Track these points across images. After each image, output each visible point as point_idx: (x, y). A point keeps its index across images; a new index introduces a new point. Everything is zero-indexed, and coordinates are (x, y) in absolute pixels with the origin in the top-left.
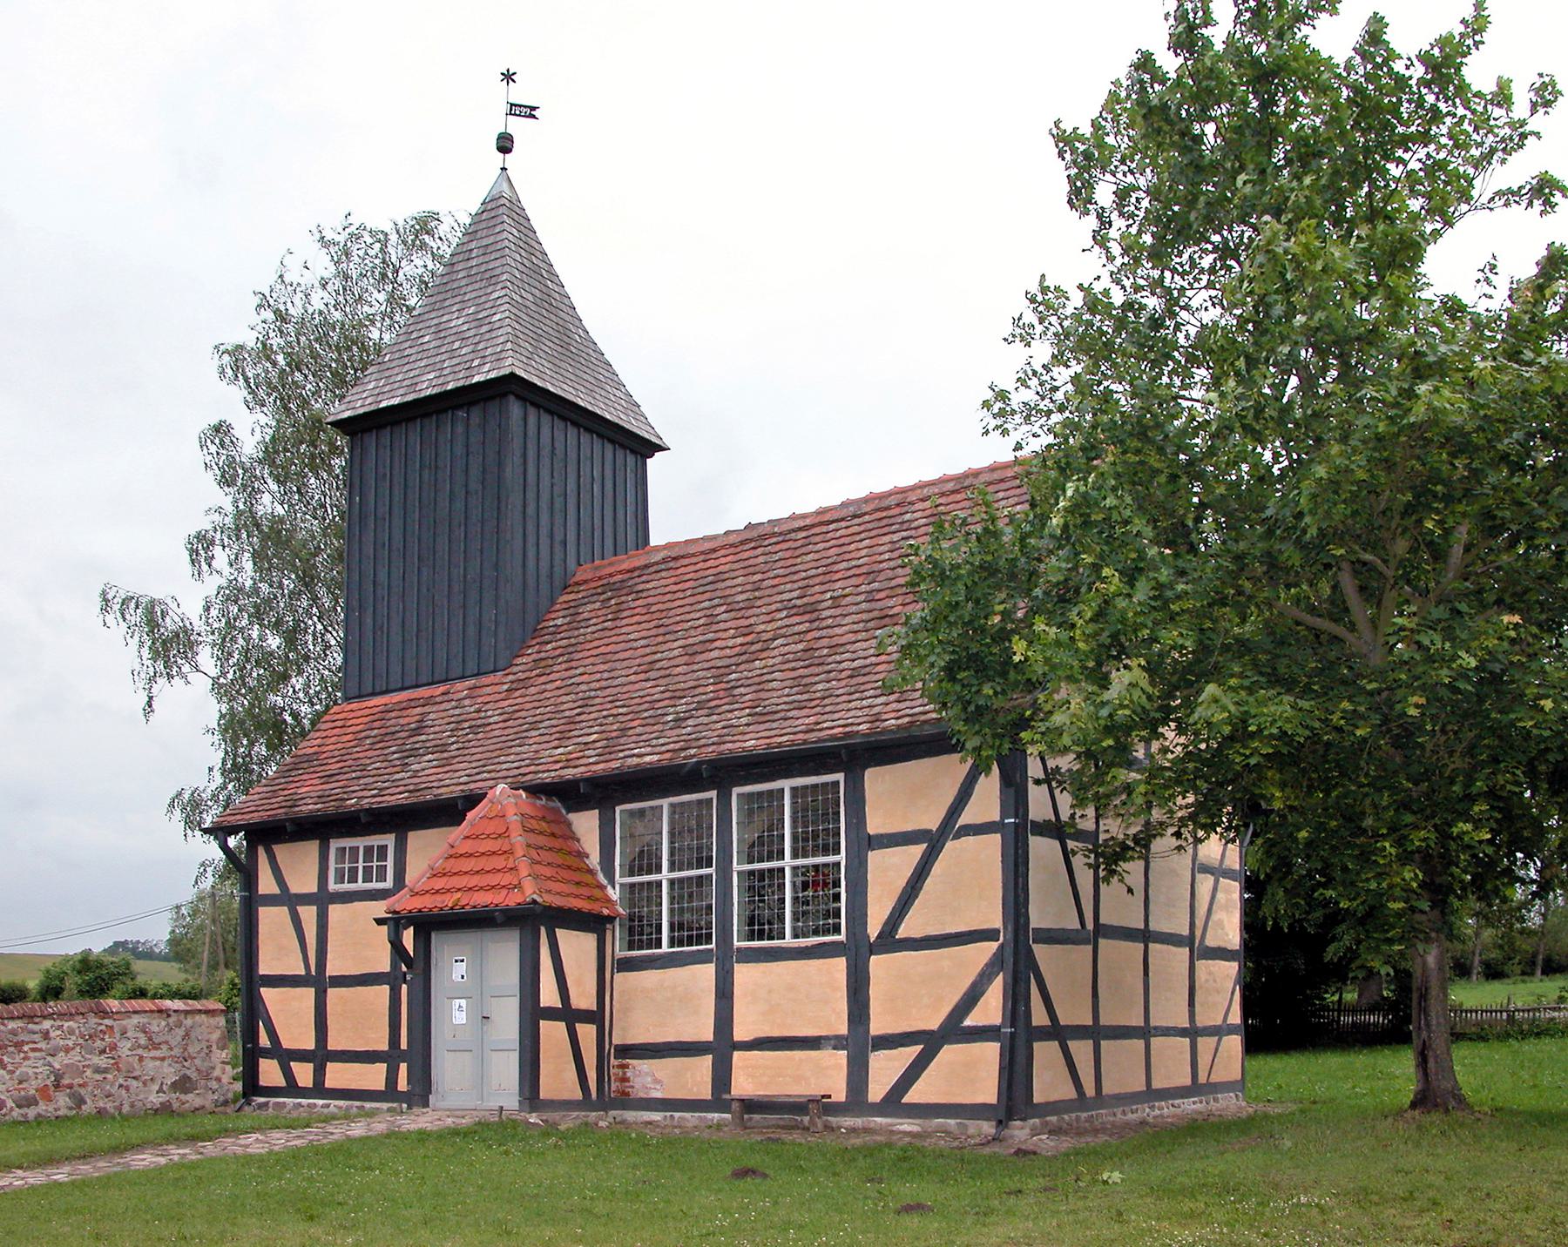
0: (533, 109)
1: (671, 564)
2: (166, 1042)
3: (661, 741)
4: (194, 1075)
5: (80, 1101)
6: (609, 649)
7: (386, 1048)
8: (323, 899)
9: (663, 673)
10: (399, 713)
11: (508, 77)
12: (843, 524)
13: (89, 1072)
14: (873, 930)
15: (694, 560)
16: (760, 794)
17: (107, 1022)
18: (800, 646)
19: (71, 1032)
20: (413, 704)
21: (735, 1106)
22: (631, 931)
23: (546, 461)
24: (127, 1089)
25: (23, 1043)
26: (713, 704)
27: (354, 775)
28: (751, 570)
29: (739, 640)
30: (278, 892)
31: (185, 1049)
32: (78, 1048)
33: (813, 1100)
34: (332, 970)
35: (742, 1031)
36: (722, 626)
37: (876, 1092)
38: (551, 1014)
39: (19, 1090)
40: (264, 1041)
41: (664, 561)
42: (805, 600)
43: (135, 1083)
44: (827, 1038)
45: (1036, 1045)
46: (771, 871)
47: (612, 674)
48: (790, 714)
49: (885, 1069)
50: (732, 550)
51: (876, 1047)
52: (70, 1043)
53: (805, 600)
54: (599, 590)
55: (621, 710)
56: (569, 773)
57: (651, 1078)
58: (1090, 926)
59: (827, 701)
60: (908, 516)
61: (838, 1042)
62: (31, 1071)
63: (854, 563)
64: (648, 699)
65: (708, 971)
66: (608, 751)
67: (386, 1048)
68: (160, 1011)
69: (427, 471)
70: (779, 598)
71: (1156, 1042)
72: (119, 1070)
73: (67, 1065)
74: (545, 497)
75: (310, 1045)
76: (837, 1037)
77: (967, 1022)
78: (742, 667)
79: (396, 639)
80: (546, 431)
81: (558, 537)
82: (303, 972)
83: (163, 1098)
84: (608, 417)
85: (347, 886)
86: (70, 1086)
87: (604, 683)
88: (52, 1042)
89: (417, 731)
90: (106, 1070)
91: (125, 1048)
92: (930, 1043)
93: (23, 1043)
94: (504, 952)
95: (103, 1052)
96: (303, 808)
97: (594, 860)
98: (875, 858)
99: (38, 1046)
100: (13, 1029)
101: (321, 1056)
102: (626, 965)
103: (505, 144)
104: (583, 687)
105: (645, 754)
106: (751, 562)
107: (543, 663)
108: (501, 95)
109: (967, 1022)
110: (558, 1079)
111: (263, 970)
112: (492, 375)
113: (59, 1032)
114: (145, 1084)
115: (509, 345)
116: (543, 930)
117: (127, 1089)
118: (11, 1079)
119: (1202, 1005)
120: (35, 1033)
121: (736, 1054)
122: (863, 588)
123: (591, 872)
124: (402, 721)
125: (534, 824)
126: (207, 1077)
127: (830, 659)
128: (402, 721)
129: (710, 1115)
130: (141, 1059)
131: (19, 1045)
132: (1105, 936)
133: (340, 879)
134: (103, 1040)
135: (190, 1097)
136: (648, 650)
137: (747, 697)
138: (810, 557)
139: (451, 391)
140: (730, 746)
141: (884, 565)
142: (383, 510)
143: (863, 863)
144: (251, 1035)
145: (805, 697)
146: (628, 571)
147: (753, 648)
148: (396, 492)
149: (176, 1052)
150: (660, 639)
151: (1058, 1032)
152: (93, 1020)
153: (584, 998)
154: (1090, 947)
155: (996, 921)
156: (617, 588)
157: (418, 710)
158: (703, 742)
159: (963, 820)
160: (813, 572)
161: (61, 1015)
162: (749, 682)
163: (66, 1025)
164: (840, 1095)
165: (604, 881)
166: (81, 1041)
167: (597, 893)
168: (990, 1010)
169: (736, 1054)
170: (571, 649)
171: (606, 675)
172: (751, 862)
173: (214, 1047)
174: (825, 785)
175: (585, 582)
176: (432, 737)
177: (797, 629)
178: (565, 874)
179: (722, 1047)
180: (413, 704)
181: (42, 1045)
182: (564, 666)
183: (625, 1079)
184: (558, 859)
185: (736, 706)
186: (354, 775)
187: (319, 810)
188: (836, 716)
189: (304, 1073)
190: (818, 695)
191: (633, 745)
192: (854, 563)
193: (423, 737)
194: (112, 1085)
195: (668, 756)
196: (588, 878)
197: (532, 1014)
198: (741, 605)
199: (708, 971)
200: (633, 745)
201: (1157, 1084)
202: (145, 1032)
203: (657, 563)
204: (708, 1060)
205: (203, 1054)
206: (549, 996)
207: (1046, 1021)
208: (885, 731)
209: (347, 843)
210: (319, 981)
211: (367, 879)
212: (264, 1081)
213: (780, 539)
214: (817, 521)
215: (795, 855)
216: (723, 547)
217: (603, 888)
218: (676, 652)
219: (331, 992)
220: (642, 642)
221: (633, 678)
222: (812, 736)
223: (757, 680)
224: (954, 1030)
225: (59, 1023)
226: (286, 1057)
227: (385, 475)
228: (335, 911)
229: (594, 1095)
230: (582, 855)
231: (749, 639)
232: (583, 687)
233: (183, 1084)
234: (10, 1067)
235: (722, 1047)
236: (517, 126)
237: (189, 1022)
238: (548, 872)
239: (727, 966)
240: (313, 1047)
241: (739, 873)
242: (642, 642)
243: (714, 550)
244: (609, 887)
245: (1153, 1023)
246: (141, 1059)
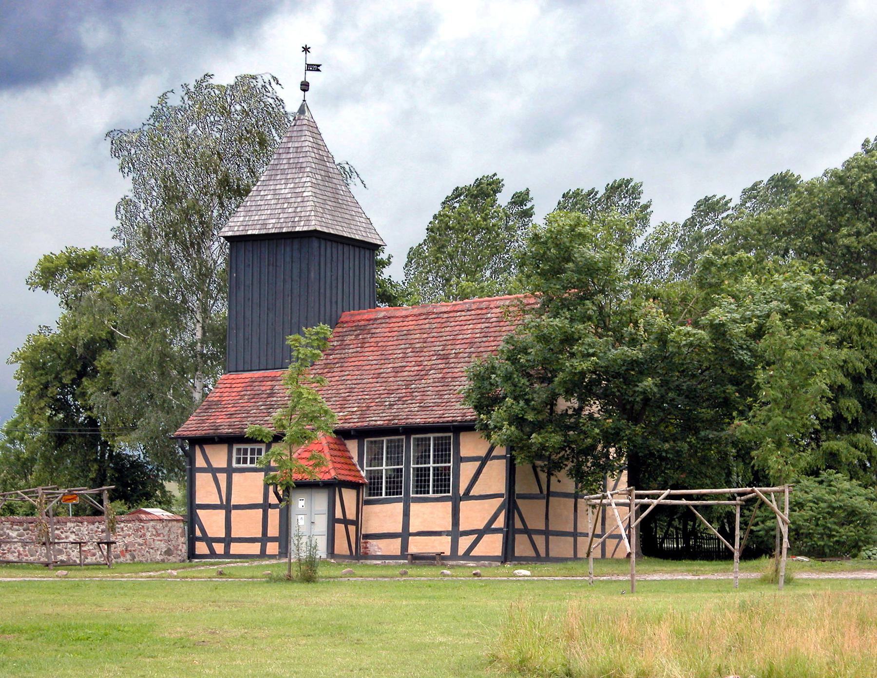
0: (319, 66)
1: (387, 320)
3: (384, 415)
5: (134, 557)
6: (360, 363)
7: (260, 536)
8: (229, 471)
9: (384, 380)
10: (260, 384)
11: (306, 49)
12: (463, 313)
14: (462, 492)
15: (398, 320)
16: (422, 439)
17: (142, 524)
18: (440, 376)
20: (266, 379)
21: (409, 557)
22: (370, 489)
23: (329, 265)
26: (404, 399)
27: (244, 415)
28: (423, 331)
29: (416, 368)
30: (217, 474)
33: (439, 554)
34: (234, 502)
35: (412, 529)
36: (410, 359)
37: (461, 551)
38: (339, 521)
40: (198, 533)
41: (384, 318)
42: (444, 352)
44: (444, 532)
45: (516, 535)
46: (425, 468)
47: (362, 377)
48: (434, 408)
49: (464, 543)
50: (415, 318)
51: (461, 535)
53: (444, 352)
54: (354, 329)
55: (367, 397)
56: (347, 425)
57: (377, 547)
58: (545, 492)
59: (448, 404)
60: (489, 315)
61: (448, 533)
63: (465, 336)
64: (378, 392)
66: (362, 417)
67: (260, 536)
69: (271, 267)
70: (434, 349)
74: (328, 281)
75: (222, 535)
76: (448, 532)
77: (493, 527)
78: (417, 382)
79: (255, 345)
80: (329, 251)
81: (334, 300)
82: (219, 503)
83: (162, 557)
84: (357, 237)
85: (242, 465)
86: (130, 551)
87: (358, 381)
89: (271, 395)
90: (142, 545)
92: (480, 534)
94: (321, 501)
95: (141, 537)
96: (223, 431)
97: (355, 460)
98: (462, 465)
101: (228, 540)
102: (368, 502)
104: (349, 382)
105: (377, 420)
106: (423, 326)
107: (329, 366)
108: (300, 60)
109: (493, 527)
110: (341, 547)
111: (198, 502)
112: (305, 229)
115: (313, 213)
116: (337, 489)
119: (609, 525)
121: (410, 538)
122: (467, 350)
123: (354, 465)
124: (262, 388)
125: (332, 446)
127: (451, 384)
128: (262, 388)
129: (400, 561)
130: (154, 540)
132: (552, 496)
133: (238, 462)
135: (171, 557)
136: (377, 367)
137: (418, 398)
138: (448, 329)
139: (285, 233)
140: (410, 420)
141: (476, 340)
142: (249, 282)
143: (459, 467)
144: (192, 531)
145: (440, 401)
146: (367, 320)
147: (421, 375)
148: (255, 274)
149: (166, 538)
150: (383, 362)
151: (528, 532)
152: (138, 523)
153: (351, 515)
154: (545, 501)
155: (503, 491)
156: (363, 329)
157: (269, 383)
158: (400, 417)
159: (493, 454)
160: (448, 338)
162: (420, 390)
164: (448, 552)
165: (360, 469)
167: (357, 474)
168: (500, 523)
169: (410, 538)
170: (342, 360)
171: (359, 377)
172: (417, 464)
174: (446, 437)
175: (347, 322)
176: (279, 399)
177: (440, 366)
178: (345, 466)
179: (405, 535)
180: (266, 379)
182: (339, 369)
183: (366, 548)
184: (342, 460)
185: (414, 401)
186: (244, 415)
187: (231, 433)
188: (451, 411)
189: (219, 548)
190: (445, 400)
191: (372, 415)
192: (465, 336)
193: (275, 399)
195: (386, 422)
196: (352, 467)
197: (332, 521)
198: (418, 350)
199: (400, 506)
200: (372, 415)
203: (381, 318)
204: (400, 540)
206: (339, 514)
207: (521, 527)
208: (466, 421)
209: (242, 446)
210: (227, 507)
211: (252, 462)
212: (198, 552)
213: (436, 316)
214: (452, 309)
216: (411, 315)
217: (359, 471)
218: (389, 370)
219: (233, 512)
220: (375, 362)
221: (371, 380)
222: (441, 420)
223: (422, 390)
224: (489, 529)
226: (209, 541)
227: (249, 265)
228: (236, 477)
230: (351, 458)
231: (420, 368)
232: (349, 382)
235: (405, 535)
236: (311, 77)
237: (170, 525)
238: (339, 466)
240: (224, 536)
241: (413, 468)
242: (375, 362)
243: (407, 317)
245: (579, 531)
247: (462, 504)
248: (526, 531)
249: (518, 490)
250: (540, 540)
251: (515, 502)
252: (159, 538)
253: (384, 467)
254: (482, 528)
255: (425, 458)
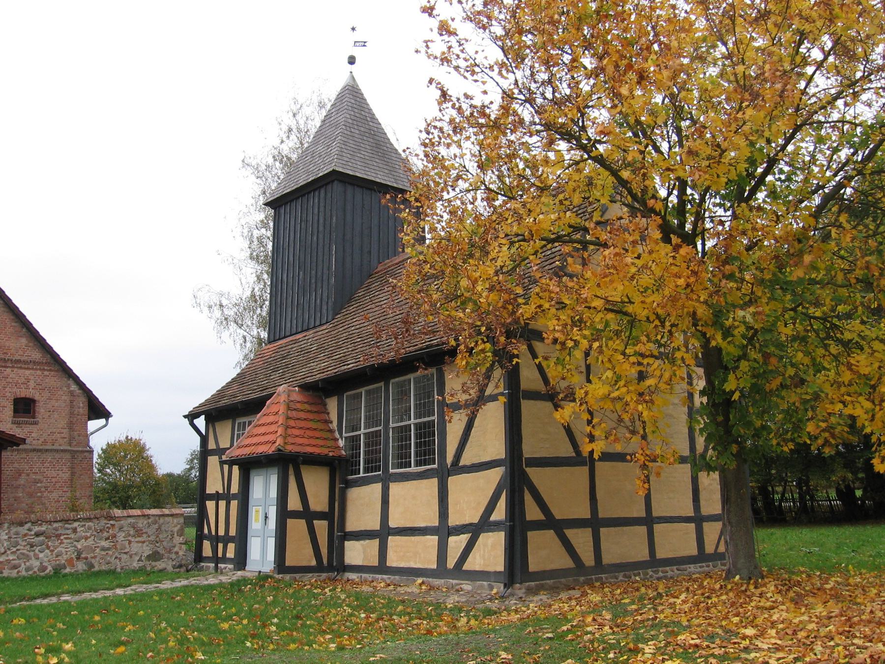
0: (365, 42)
2: (146, 533)
4: (162, 552)
13: (98, 550)
17: (112, 522)
19: (90, 528)
24: (120, 559)
25: (60, 535)
31: (158, 537)
32: (93, 538)
38: (295, 515)
39: (56, 561)
43: (125, 556)
45: (529, 534)
52: (88, 534)
62: (63, 550)
65: (377, 487)
68: (144, 516)
71: (657, 528)
72: (116, 548)
73: (85, 546)
83: (141, 564)
86: (86, 558)
88: (78, 534)
90: (108, 549)
91: (121, 536)
92: (475, 530)
93: (60, 535)
95: (106, 539)
99: (69, 536)
100: (56, 527)
103: (352, 61)
113: (82, 529)
114: (131, 556)
117: (120, 559)
118: (52, 554)
120: (68, 529)
123: (331, 431)
126: (170, 552)
130: (130, 542)
131: (58, 536)
134: (108, 532)
135: (157, 563)
161: (85, 519)
163: (87, 524)
166: (95, 533)
168: (499, 513)
173: (176, 534)
181: (72, 536)
194: (111, 556)
199: (377, 487)
201: (660, 554)
202: (134, 528)
205: (168, 539)
207: (541, 516)
215: (415, 418)
217: (336, 440)
224: (484, 525)
225: (83, 523)
229: (325, 561)
233: (155, 556)
234: (52, 548)
237: (162, 520)
239: (387, 485)
244: (340, 440)
246: (130, 542)
247: (453, 482)
248: (550, 523)
249: (529, 450)
250: (581, 539)
251: (524, 475)
252: (138, 539)
253: (363, 431)
254: (476, 522)
255: (405, 414)
